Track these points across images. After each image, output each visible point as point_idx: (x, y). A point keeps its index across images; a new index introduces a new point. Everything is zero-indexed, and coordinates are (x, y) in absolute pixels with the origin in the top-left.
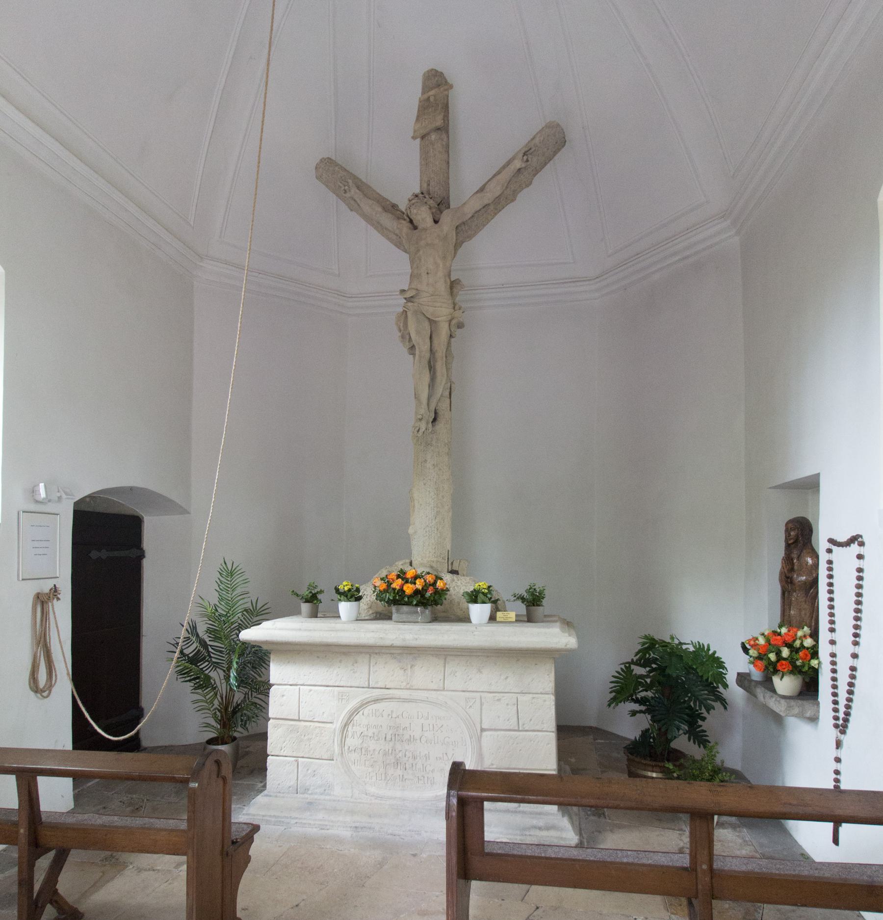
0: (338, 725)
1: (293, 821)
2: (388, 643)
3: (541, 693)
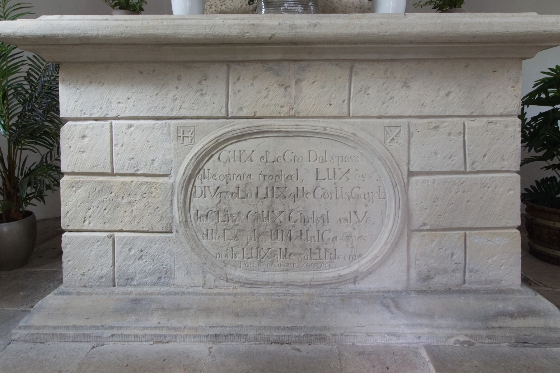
0: (178, 178)
1: (107, 333)
3: (501, 116)
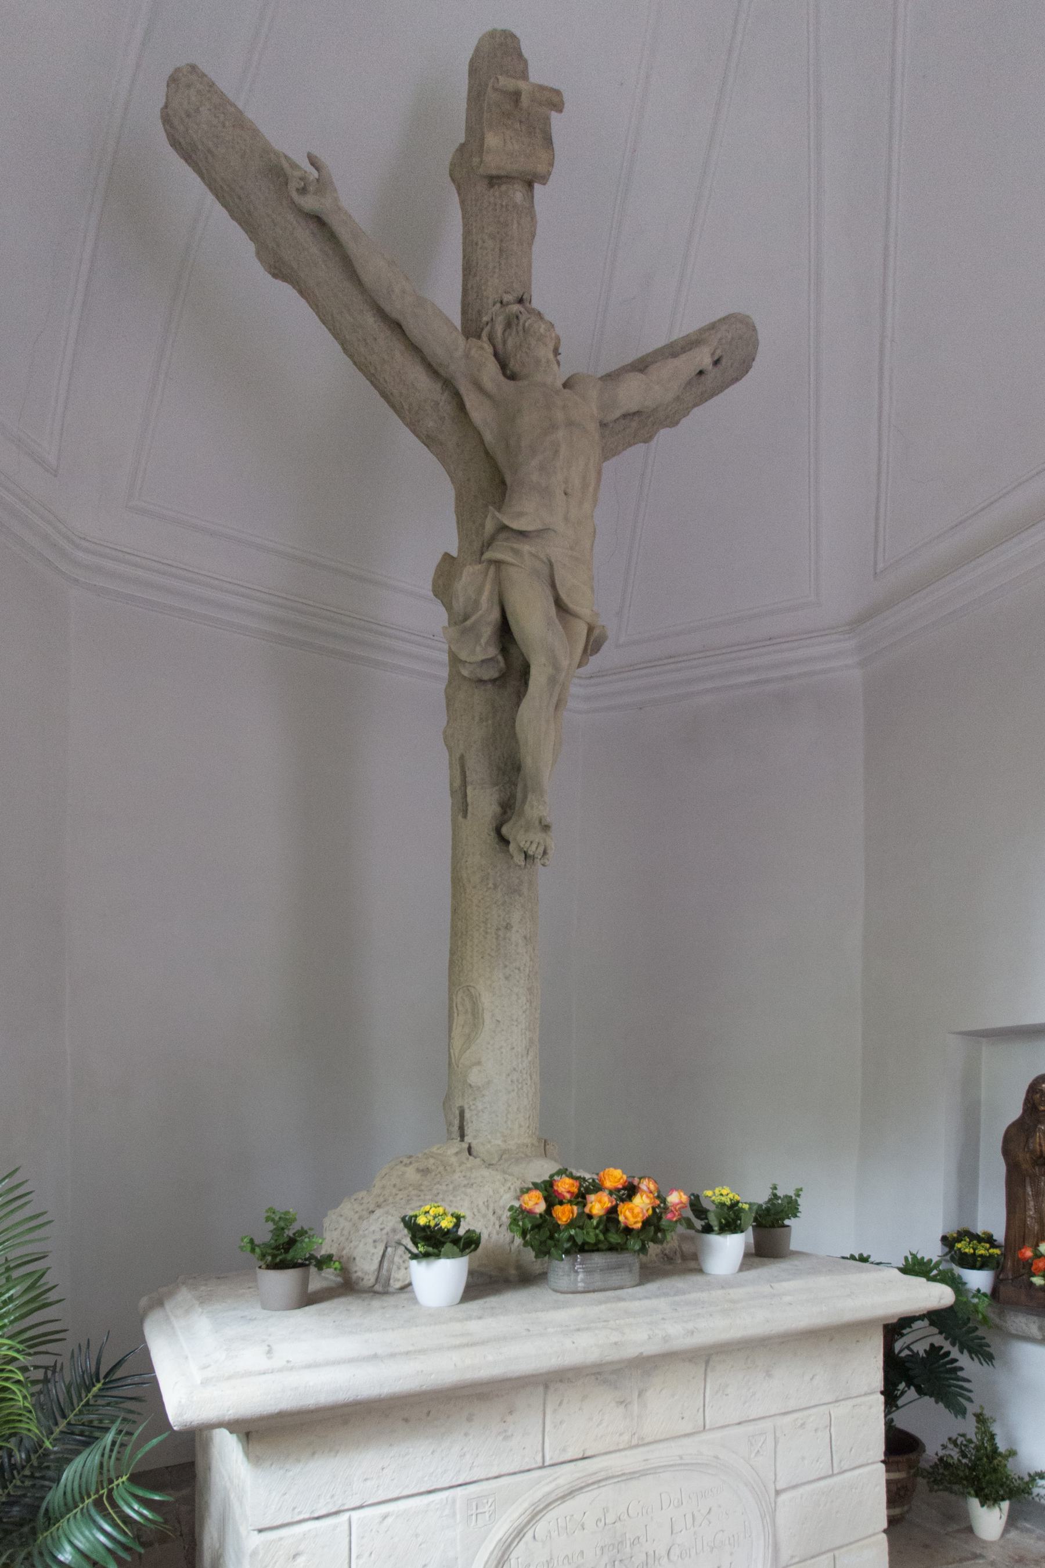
2: (631, 1352)
3: (865, 1394)
